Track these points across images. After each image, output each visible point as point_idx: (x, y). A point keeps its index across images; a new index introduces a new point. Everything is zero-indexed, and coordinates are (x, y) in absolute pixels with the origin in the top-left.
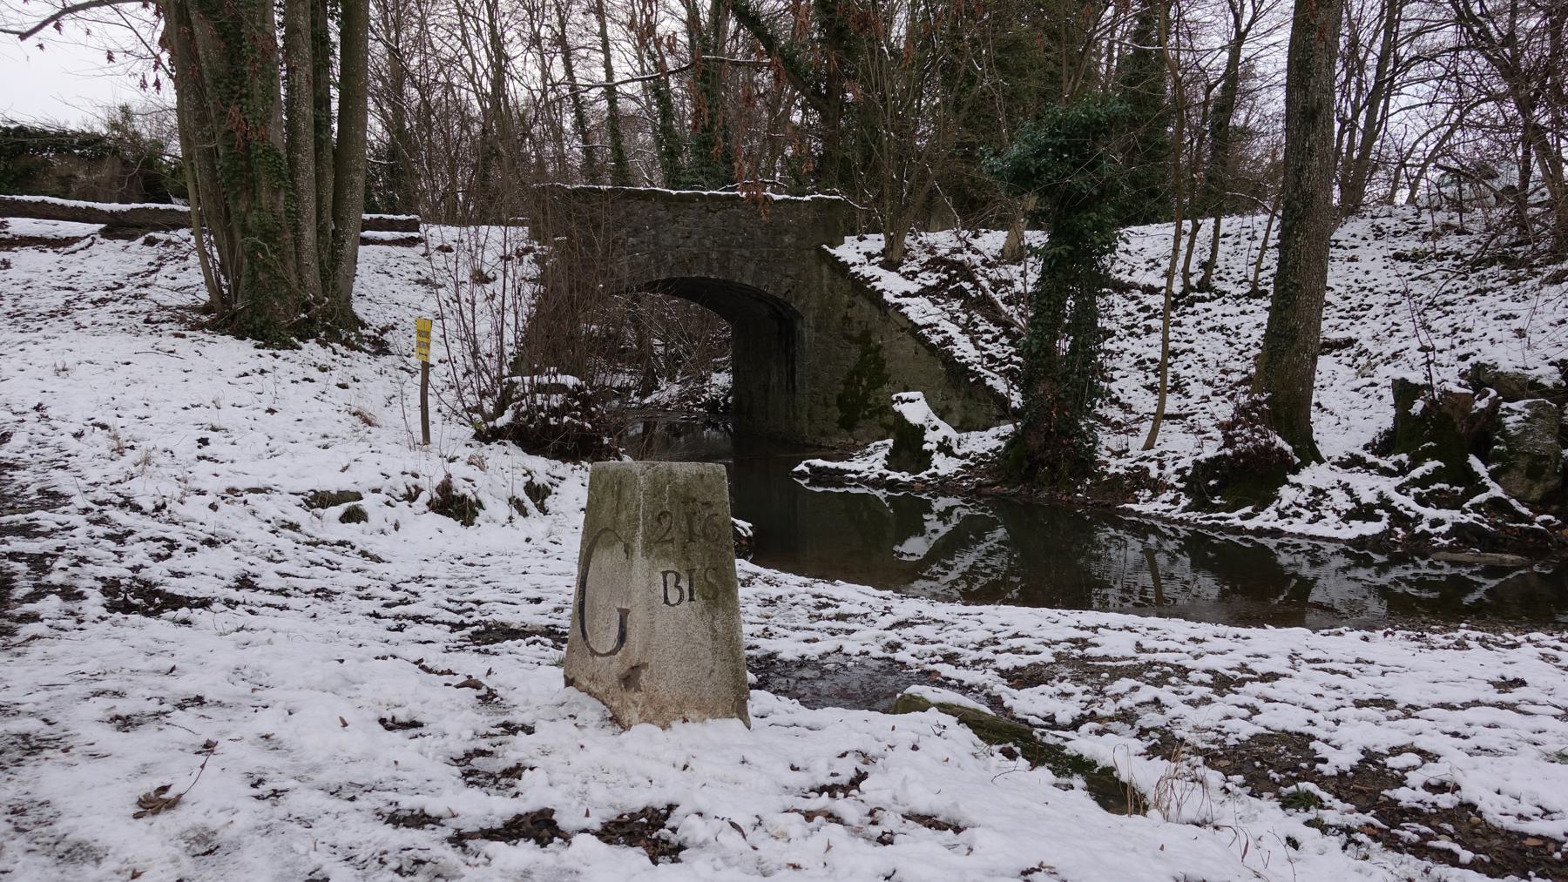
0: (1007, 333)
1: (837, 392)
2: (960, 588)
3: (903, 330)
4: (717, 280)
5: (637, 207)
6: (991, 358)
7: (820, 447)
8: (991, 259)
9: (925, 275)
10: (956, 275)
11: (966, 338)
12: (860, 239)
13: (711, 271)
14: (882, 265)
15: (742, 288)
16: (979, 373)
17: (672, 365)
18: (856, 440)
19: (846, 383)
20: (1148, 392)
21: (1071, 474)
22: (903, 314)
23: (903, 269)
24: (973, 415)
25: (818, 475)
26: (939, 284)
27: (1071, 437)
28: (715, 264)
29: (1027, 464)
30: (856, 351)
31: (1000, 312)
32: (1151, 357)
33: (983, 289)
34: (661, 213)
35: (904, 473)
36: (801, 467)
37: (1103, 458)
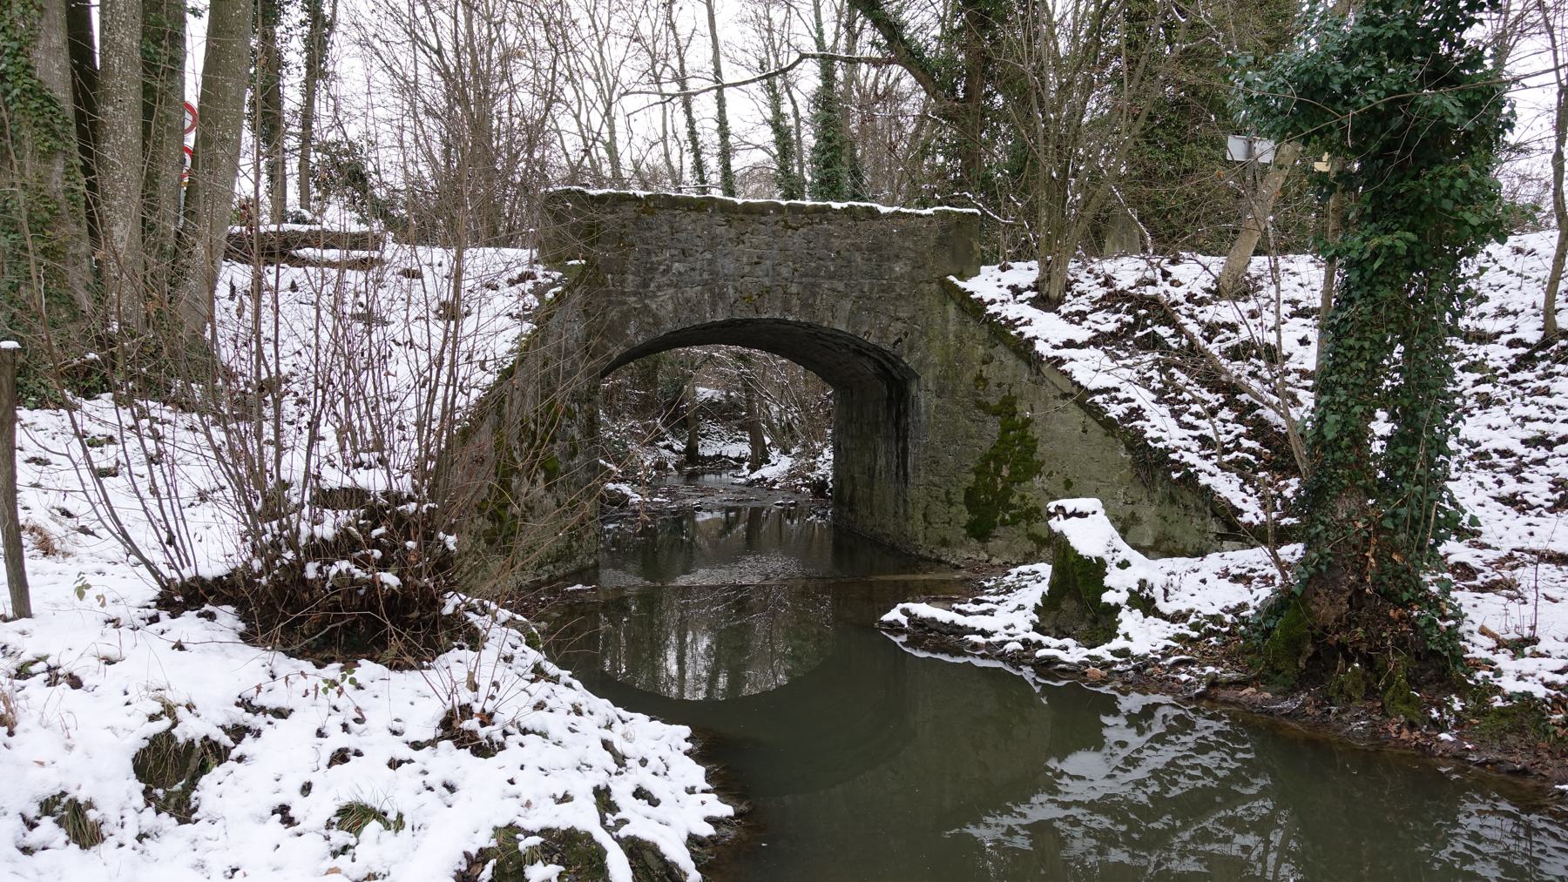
0: (1230, 403)
1: (965, 484)
2: (1150, 791)
3: (1065, 396)
4: (797, 324)
5: (686, 221)
6: (1205, 441)
7: (939, 561)
8: (1200, 294)
9: (1099, 316)
10: (1146, 317)
11: (1165, 409)
12: (1003, 269)
13: (789, 311)
14: (1034, 303)
15: (835, 335)
16: (1187, 465)
17: (786, 437)
18: (991, 556)
19: (977, 472)
20: (1507, 508)
21: (1413, 682)
22: (1065, 373)
23: (1064, 309)
24: (1177, 531)
25: (922, 630)
26: (1120, 329)
27: (1406, 605)
28: (795, 301)
29: (1310, 648)
30: (993, 427)
31: (1219, 370)
32: (1501, 447)
33: (1190, 337)
34: (720, 230)
35: (1068, 641)
36: (894, 615)
37: (1480, 653)
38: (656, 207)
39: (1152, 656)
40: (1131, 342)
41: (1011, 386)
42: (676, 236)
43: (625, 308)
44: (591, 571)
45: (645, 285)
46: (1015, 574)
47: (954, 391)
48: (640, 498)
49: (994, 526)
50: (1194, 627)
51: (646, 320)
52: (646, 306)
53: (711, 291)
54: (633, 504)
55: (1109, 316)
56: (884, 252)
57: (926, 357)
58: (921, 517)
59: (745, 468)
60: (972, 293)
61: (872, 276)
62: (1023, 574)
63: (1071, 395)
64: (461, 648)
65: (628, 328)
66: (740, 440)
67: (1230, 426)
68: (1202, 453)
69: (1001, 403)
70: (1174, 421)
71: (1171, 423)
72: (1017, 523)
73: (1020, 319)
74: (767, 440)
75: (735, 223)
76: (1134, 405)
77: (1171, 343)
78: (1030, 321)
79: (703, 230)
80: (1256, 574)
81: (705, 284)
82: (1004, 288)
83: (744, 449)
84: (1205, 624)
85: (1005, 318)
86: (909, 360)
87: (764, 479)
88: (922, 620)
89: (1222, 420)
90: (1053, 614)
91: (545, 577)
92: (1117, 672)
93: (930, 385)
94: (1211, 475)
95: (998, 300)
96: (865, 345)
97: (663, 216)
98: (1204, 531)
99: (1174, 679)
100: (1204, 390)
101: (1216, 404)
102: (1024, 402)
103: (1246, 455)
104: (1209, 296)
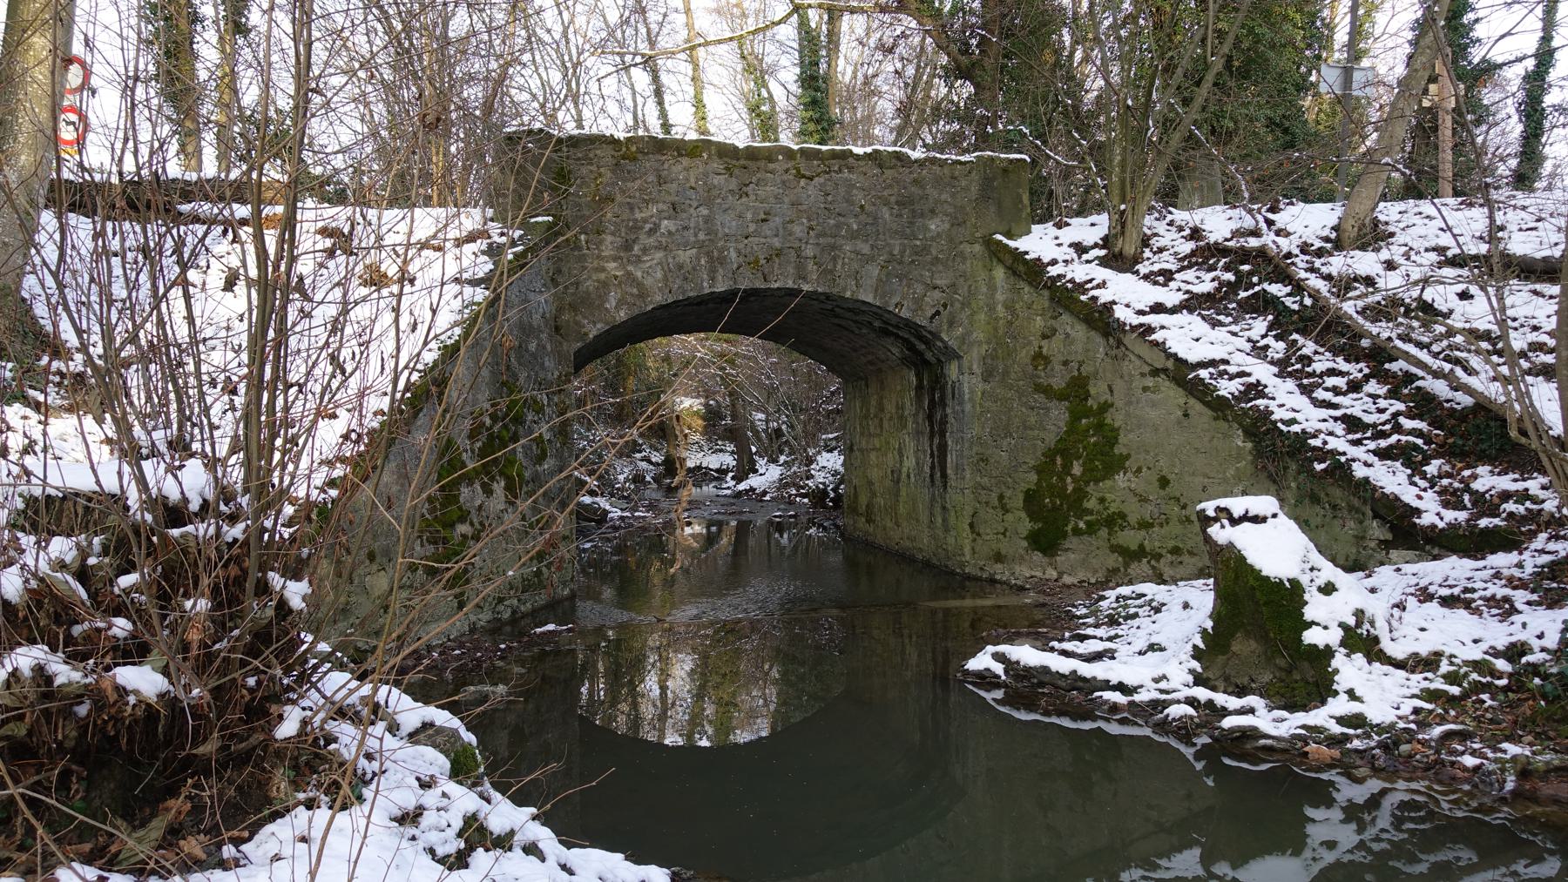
1: (1024, 486)
3: (1155, 372)
5: (679, 169)
7: (992, 581)
8: (1318, 244)
9: (1190, 275)
10: (1251, 273)
12: (1059, 226)
13: (804, 279)
14: (1104, 262)
16: (1334, 453)
17: (774, 445)
18: (1061, 574)
19: (1039, 470)
22: (1156, 344)
23: (1143, 268)
26: (1218, 290)
28: (811, 266)
30: (1059, 415)
31: (1359, 335)
33: (1315, 295)
34: (717, 180)
36: (982, 661)
38: (639, 151)
39: (1401, 725)
40: (1234, 305)
41: (1081, 364)
42: (664, 187)
43: (602, 276)
44: (566, 603)
45: (627, 247)
46: (1113, 599)
47: (1006, 373)
48: (619, 513)
49: (1065, 535)
50: (1451, 678)
51: (629, 290)
52: (629, 274)
53: (708, 254)
54: (612, 519)
55: (1202, 274)
56: (917, 207)
57: (968, 333)
58: (967, 527)
59: (728, 479)
60: (1027, 253)
61: (904, 236)
62: (1125, 598)
63: (1165, 370)
64: (310, 805)
65: (607, 300)
66: (721, 451)
67: (1383, 403)
68: (1350, 437)
69: (1068, 385)
70: (1305, 399)
71: (1301, 401)
72: (1095, 532)
73: (1091, 281)
74: (754, 449)
75: (736, 171)
76: (1252, 380)
77: (1288, 304)
78: (1104, 283)
79: (697, 180)
80: (1476, 596)
81: (700, 246)
82: (1065, 246)
83: (729, 460)
84: (1466, 675)
85: (1072, 281)
86: (949, 338)
87: (752, 489)
88: (1028, 669)
89: (1370, 395)
90: (1221, 659)
91: (506, 615)
92: (1356, 751)
93: (975, 367)
94: (1367, 464)
95: (1060, 260)
96: (894, 321)
97: (649, 163)
98: (1363, 538)
99: (1453, 763)
100: (1340, 360)
101: (1360, 375)
102: (1100, 383)
103: (1410, 438)
104: (1329, 246)
